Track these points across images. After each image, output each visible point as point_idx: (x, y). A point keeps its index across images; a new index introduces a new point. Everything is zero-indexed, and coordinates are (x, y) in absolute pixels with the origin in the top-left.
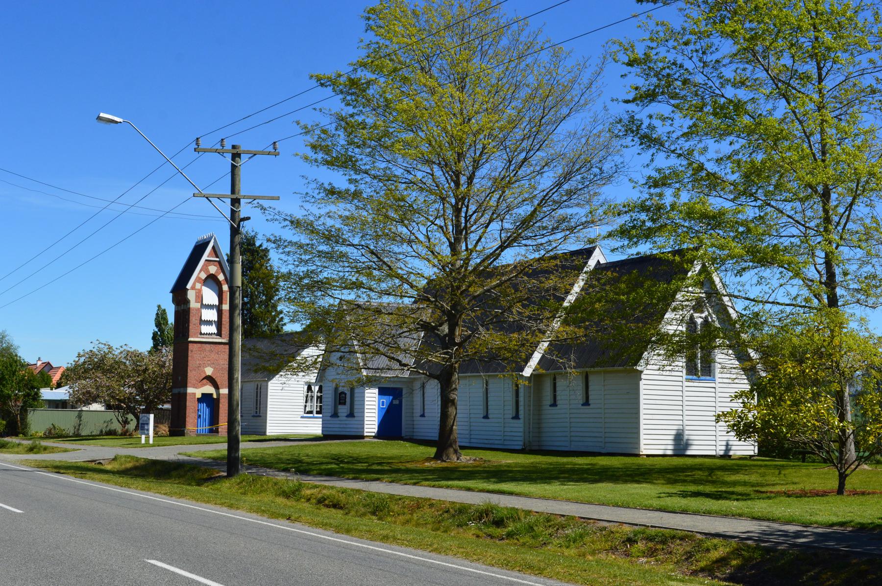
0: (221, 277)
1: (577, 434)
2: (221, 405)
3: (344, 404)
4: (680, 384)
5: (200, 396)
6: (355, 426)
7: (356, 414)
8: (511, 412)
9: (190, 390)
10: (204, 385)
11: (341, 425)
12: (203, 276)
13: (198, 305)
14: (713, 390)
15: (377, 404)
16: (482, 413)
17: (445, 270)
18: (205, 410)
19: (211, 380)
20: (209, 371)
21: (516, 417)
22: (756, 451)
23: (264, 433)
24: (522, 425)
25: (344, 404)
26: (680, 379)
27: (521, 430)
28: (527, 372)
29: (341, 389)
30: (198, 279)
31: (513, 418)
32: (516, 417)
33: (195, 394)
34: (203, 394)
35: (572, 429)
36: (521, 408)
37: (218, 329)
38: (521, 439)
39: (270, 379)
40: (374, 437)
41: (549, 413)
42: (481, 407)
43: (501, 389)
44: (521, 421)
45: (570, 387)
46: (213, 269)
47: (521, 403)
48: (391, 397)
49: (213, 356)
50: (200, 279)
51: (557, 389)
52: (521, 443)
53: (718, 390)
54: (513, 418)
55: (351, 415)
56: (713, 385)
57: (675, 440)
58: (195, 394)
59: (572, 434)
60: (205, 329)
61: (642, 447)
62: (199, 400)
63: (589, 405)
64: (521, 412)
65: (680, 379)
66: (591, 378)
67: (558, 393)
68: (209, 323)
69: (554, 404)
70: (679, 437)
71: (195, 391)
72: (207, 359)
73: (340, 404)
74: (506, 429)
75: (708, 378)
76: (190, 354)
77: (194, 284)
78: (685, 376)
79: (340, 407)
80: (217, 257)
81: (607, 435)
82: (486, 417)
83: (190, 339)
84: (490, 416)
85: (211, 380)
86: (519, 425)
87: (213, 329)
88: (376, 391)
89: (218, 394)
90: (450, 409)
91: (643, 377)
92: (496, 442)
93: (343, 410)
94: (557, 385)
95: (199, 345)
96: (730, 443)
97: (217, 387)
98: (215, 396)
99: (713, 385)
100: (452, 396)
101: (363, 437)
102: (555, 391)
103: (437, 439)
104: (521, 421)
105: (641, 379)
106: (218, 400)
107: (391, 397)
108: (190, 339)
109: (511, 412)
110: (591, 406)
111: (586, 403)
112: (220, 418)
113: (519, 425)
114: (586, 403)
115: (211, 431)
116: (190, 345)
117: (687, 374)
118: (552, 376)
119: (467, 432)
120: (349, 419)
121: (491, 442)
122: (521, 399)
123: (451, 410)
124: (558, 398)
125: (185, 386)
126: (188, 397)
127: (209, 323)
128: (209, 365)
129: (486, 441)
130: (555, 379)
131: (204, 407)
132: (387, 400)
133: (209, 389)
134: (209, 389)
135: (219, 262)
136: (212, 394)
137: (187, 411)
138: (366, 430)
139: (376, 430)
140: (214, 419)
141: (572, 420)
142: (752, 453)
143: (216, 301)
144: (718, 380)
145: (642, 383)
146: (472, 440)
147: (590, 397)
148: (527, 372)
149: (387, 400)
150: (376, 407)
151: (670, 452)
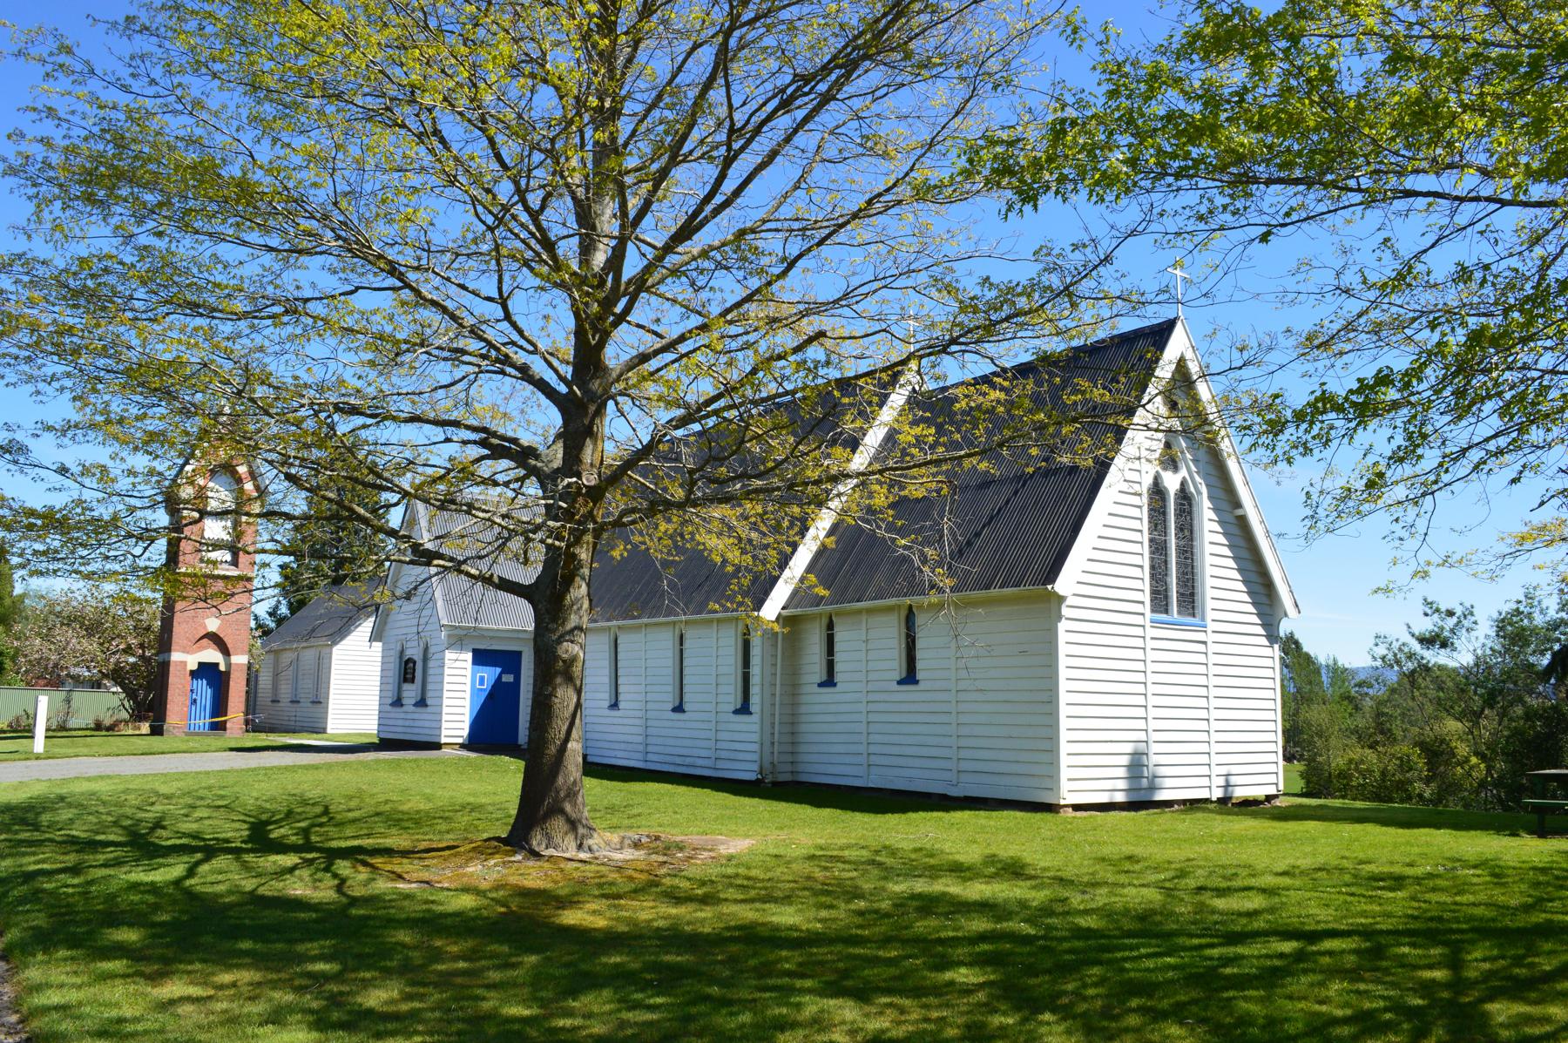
1: (887, 750)
3: (412, 681)
4: (1139, 631)
5: (195, 667)
6: (427, 724)
7: (429, 702)
8: (731, 698)
9: (176, 657)
11: (408, 723)
14: (1201, 648)
15: (468, 681)
16: (670, 700)
18: (204, 691)
19: (216, 640)
21: (744, 709)
22: (1281, 787)
23: (324, 731)
24: (756, 728)
25: (412, 681)
26: (1138, 620)
27: (756, 737)
28: (771, 609)
29: (409, 653)
31: (736, 712)
32: (744, 709)
35: (873, 738)
36: (755, 690)
38: (755, 757)
39: (335, 643)
40: (462, 746)
41: (816, 699)
42: (670, 689)
43: (712, 651)
44: (755, 718)
45: (867, 646)
47: (755, 680)
48: (499, 670)
51: (837, 648)
52: (756, 767)
53: (1212, 648)
54: (736, 712)
55: (422, 703)
56: (1201, 636)
57: (1130, 767)
58: (184, 663)
59: (873, 749)
61: (1065, 785)
62: (193, 674)
63: (835, 685)
64: (755, 700)
65: (1138, 620)
66: (920, 619)
67: (838, 657)
69: (829, 682)
70: (1136, 765)
73: (405, 680)
74: (721, 736)
75: (1190, 620)
78: (1148, 614)
79: (406, 686)
81: (963, 754)
82: (679, 709)
84: (686, 707)
85: (216, 640)
86: (749, 727)
88: (469, 656)
89: (229, 665)
90: (560, 692)
91: (1065, 611)
92: (700, 762)
93: (411, 692)
94: (837, 639)
96: (1233, 780)
97: (226, 652)
98: (222, 668)
99: (1201, 636)
100: (568, 649)
101: (437, 746)
102: (830, 650)
103: (521, 764)
104: (755, 718)
105: (1060, 617)
106: (227, 674)
107: (499, 670)
109: (733, 699)
110: (921, 686)
111: (910, 678)
112: (231, 704)
113: (749, 727)
114: (910, 678)
117: (1153, 611)
118: (825, 621)
119: (640, 739)
120: (419, 710)
121: (688, 761)
122: (755, 670)
123: (564, 697)
124: (838, 667)
125: (169, 650)
129: (678, 760)
130: (830, 626)
132: (490, 674)
133: (212, 655)
134: (212, 655)
138: (444, 732)
139: (465, 733)
140: (220, 705)
141: (872, 717)
142: (1272, 791)
144: (1211, 626)
145: (1062, 626)
146: (651, 757)
147: (919, 665)
148: (771, 609)
149: (490, 674)
150: (468, 688)
151: (1120, 797)
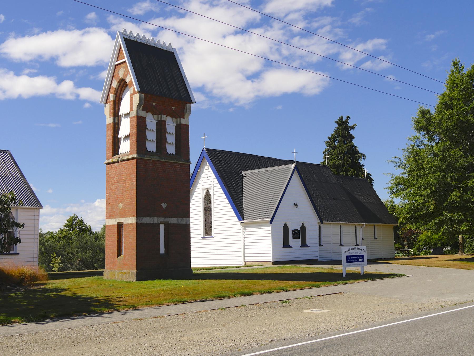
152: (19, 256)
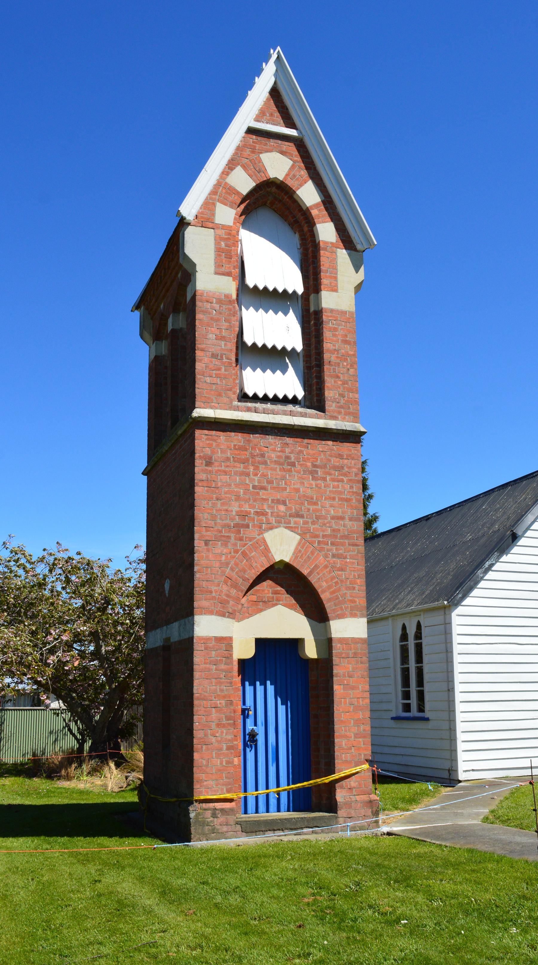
0: (308, 195)
2: (338, 689)
5: (248, 651)
9: (206, 626)
10: (268, 604)
12: (243, 183)
13: (229, 286)
17: (178, 890)
19: (291, 581)
20: (282, 545)
30: (222, 191)
33: (226, 642)
34: (260, 643)
37: (306, 385)
46: (278, 165)
49: (299, 483)
50: (232, 190)
58: (226, 642)
60: (257, 380)
61: (462, 766)
62: (249, 670)
68: (271, 357)
71: (229, 630)
72: (270, 494)
76: (200, 472)
77: (209, 205)
80: (290, 123)
83: (197, 413)
85: (291, 581)
87: (288, 383)
89: (326, 643)
95: (238, 438)
97: (316, 610)
98: (311, 651)
106: (324, 666)
108: (197, 413)
115: (302, 801)
116: (203, 440)
126: (198, 658)
127: (271, 357)
128: (281, 521)
131: (265, 696)
133: (286, 621)
134: (286, 621)
135: (300, 145)
136: (296, 644)
137: (198, 721)
143: (291, 279)
152: (430, 725)
